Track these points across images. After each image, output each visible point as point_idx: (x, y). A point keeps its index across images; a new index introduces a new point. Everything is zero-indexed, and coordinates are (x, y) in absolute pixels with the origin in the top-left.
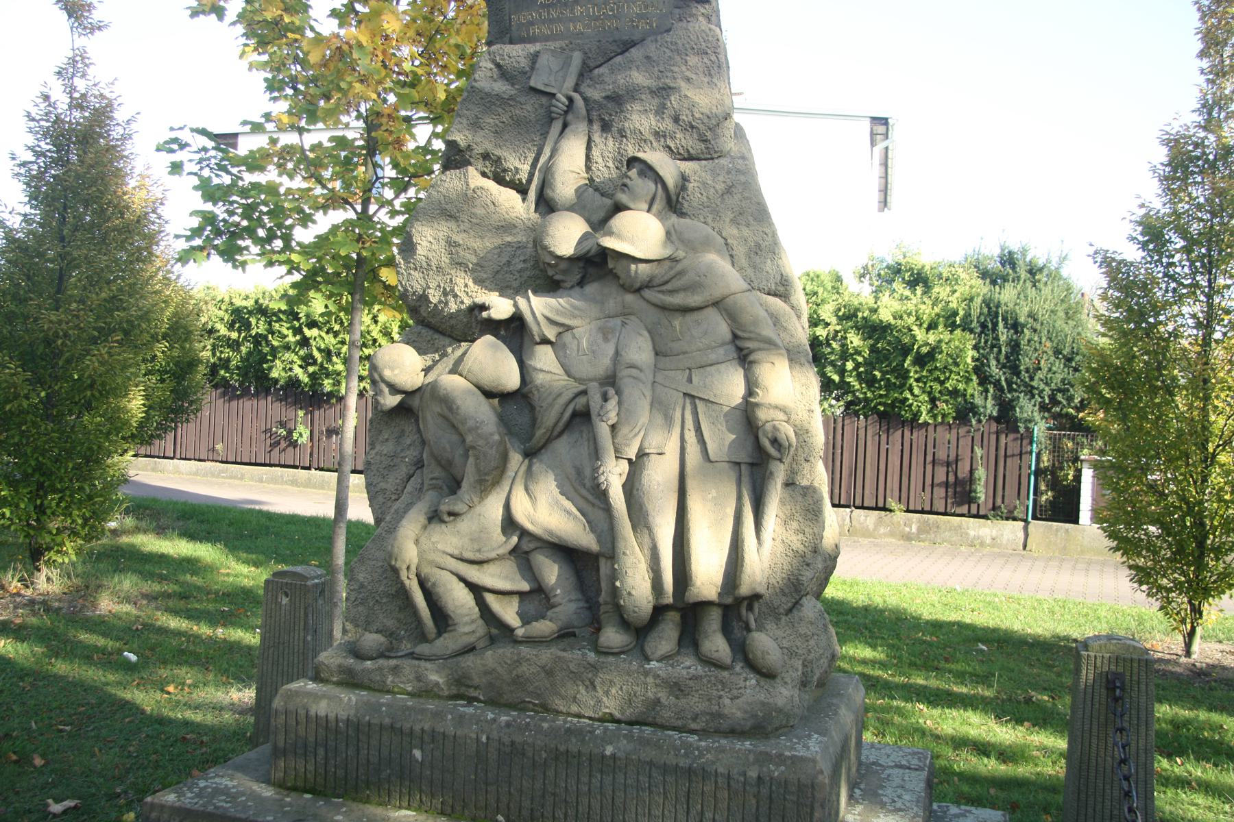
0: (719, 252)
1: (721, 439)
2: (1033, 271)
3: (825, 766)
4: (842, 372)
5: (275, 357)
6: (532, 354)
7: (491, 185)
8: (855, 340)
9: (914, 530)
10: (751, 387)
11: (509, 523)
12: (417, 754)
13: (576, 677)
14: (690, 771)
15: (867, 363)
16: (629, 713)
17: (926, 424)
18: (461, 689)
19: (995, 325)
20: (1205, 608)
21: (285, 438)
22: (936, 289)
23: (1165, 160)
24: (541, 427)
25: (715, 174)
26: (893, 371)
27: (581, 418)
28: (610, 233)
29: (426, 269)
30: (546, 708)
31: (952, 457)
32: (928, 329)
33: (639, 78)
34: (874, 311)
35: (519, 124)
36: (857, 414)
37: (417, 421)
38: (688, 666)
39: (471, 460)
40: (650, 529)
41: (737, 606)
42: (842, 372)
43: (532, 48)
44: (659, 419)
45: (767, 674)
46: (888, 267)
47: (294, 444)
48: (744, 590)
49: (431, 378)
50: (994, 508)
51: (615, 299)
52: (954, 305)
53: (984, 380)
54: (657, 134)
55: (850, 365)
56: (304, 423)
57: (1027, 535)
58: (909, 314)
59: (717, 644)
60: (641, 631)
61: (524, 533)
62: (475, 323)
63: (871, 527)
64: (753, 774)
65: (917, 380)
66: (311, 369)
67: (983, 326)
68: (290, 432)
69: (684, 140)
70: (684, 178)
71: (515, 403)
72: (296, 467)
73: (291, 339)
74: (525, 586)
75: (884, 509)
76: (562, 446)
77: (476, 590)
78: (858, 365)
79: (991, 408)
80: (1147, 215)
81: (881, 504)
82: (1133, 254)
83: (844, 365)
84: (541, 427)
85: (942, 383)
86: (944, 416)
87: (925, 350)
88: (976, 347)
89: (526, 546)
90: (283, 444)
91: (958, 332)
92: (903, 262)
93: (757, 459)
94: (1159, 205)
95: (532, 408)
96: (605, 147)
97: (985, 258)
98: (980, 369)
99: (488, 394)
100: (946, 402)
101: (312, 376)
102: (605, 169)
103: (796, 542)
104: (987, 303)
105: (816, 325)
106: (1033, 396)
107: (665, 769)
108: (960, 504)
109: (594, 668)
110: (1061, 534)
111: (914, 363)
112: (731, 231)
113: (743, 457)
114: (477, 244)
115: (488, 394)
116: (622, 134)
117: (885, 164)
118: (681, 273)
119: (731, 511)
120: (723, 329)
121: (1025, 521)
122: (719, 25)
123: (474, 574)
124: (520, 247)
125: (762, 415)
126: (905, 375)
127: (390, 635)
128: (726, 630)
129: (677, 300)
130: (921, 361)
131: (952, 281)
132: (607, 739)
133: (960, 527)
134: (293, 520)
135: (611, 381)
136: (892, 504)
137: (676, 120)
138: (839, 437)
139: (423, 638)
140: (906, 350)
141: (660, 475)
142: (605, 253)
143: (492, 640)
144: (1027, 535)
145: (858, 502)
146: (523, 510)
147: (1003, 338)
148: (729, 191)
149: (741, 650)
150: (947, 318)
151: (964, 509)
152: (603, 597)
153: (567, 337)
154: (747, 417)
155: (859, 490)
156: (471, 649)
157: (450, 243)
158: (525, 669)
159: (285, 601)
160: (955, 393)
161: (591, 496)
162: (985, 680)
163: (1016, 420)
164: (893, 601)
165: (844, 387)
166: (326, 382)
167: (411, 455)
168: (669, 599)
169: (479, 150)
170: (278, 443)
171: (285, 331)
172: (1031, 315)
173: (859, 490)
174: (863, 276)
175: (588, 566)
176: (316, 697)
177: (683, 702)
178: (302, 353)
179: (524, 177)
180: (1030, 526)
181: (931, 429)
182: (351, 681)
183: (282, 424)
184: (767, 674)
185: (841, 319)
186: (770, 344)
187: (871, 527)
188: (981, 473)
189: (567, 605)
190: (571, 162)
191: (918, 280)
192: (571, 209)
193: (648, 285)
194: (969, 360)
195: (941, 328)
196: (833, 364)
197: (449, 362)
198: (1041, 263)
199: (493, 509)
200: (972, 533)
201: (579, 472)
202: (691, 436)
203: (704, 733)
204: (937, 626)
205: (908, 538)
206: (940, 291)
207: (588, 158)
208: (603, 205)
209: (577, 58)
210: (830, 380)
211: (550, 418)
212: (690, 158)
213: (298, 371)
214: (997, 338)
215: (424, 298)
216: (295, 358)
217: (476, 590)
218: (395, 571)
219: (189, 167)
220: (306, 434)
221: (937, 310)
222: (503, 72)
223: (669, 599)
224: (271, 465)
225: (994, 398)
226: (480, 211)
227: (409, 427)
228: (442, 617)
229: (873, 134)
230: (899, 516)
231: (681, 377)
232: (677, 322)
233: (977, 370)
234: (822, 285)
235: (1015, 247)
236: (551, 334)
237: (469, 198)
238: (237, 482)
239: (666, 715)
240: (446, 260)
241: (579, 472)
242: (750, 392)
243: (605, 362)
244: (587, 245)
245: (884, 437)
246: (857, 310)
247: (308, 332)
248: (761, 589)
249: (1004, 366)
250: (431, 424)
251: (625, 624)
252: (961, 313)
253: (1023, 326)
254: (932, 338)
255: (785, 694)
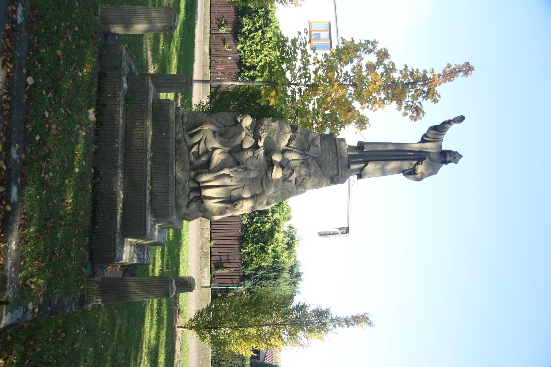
0: (275, 190)
1: (235, 193)
2: (295, 283)
3: (170, 220)
4: (257, 222)
5: (250, 19)
6: (251, 151)
7: (288, 138)
8: (268, 226)
9: (205, 250)
10: (247, 199)
11: (214, 149)
12: (164, 134)
13: (184, 167)
14: (168, 193)
15: (260, 230)
16: (177, 179)
17: (241, 252)
18: (178, 141)
19: (276, 272)
20: (193, 330)
21: (221, 23)
22: (286, 252)
23: (323, 309)
24: (235, 156)
25: (292, 188)
26: (258, 239)
27: (238, 163)
28: (277, 167)
29: (269, 125)
30: (176, 161)
31: (230, 261)
32: (273, 250)
33: (313, 170)
34: (278, 232)
35: (302, 144)
36: (243, 228)
37: (235, 125)
38: (188, 190)
39: (227, 140)
40: (215, 180)
41: (201, 199)
42: (257, 222)
43: (319, 146)
44: (238, 180)
45: (188, 207)
46: (293, 235)
47: (219, 27)
48: (204, 200)
49: (245, 129)
50: (214, 276)
51: (263, 169)
52: (281, 258)
53: (257, 270)
54: (300, 175)
55: (259, 225)
56: (227, 31)
57: (206, 287)
58: (277, 243)
59: (192, 196)
60: (194, 179)
61: (212, 152)
62: (257, 138)
63: (204, 236)
64: (169, 205)
65: (255, 248)
66: (247, 33)
67: (275, 268)
68: (223, 25)
69: (299, 180)
70: (291, 181)
71: (240, 149)
72: (210, 28)
73: (257, 25)
74: (200, 153)
75: (211, 240)
76: (231, 159)
77: (199, 142)
78: (259, 227)
79: (248, 272)
80: (306, 306)
81: (212, 238)
82: (295, 303)
83: (259, 223)
84: (235, 156)
85: (255, 256)
86: (244, 257)
87: (266, 249)
88: (268, 266)
89: (209, 153)
90: (218, 22)
91: (272, 260)
92: (296, 240)
93: (232, 201)
94: (310, 310)
95: (239, 151)
96: (297, 163)
97: (298, 268)
98: (261, 268)
99: (242, 142)
100: (249, 258)
101: (244, 33)
102: (292, 164)
103: (215, 210)
104: (283, 269)
105: (272, 212)
106: (252, 286)
107: (168, 187)
108: (214, 265)
109: (186, 171)
110: (207, 298)
111: (261, 246)
112: (280, 192)
113: (232, 198)
114: (275, 136)
115: (242, 142)
116: (300, 167)
117: (333, 234)
118: (270, 183)
119: (220, 196)
120: (258, 192)
121: (211, 286)
122: (326, 186)
123: (202, 142)
124: (275, 146)
125: (241, 202)
126: (257, 243)
127: (187, 123)
128: (195, 197)
129: (264, 182)
130: (262, 248)
131: (290, 256)
132: (172, 175)
133: (207, 265)
134: (193, 36)
135: (246, 169)
136: (213, 242)
137: (304, 179)
138: (234, 223)
139: (187, 131)
140: (265, 243)
141: (227, 181)
142: (273, 166)
143: (188, 147)
144: (206, 287)
145: (212, 231)
146: (217, 152)
147: (271, 275)
148: (289, 191)
149: (191, 202)
150: (277, 256)
151: (213, 266)
152: (200, 170)
153: (255, 159)
154: (240, 198)
155: (217, 231)
156: (186, 142)
157: (275, 130)
158: (184, 156)
159: (184, 80)
160: (252, 260)
161: (222, 166)
162: (167, 268)
163: (244, 281)
164: (184, 243)
165: (252, 223)
166: (242, 38)
167: (227, 124)
168: (201, 185)
169: (296, 135)
170: (219, 21)
171: (260, 23)
172: (279, 283)
173: (217, 231)
174: (290, 227)
175: (206, 167)
176: (173, 110)
177: (181, 190)
178: (253, 29)
179: (290, 145)
180: (208, 288)
181: (239, 253)
182: (177, 116)
183: (226, 22)
184: (188, 207)
185: (275, 221)
186: (255, 202)
187: (204, 236)
188: (226, 271)
189: (197, 163)
190: (293, 156)
191: (290, 246)
192: (283, 157)
193: (267, 176)
194: (263, 264)
195: (273, 254)
196: (259, 219)
197: (248, 132)
198: (298, 286)
199: (216, 145)
200: (205, 269)
201: (226, 164)
202: (235, 187)
203: (175, 194)
204: (178, 256)
205: (202, 248)
206: (286, 253)
207: (295, 160)
208: (283, 165)
209: (317, 156)
210: (254, 219)
211: (237, 156)
212: (296, 182)
213: (246, 28)
214: (271, 273)
215: (262, 125)
216: (250, 27)
217: (199, 142)
218: (202, 125)
219: (300, 36)
220: (223, 32)
221: (279, 252)
222: (314, 139)
223: (201, 185)
224: (210, 18)
225: (251, 273)
226: (282, 137)
227: (233, 123)
228: (192, 135)
229: (343, 228)
230: (209, 245)
231: (248, 184)
232: (259, 182)
233: (260, 267)
234: (286, 213)
235: (302, 277)
236: (255, 155)
237: (285, 134)
238: (203, 6)
239: (178, 187)
240: (271, 130)
241: (226, 164)
242: (246, 199)
243: (250, 167)
244: (275, 162)
245: (235, 238)
246: (278, 226)
247: (260, 31)
248: (205, 204)
249: (262, 275)
250: (234, 130)
251: (196, 176)
252: (279, 260)
253: (276, 281)
254: (270, 251)
255: (184, 210)
